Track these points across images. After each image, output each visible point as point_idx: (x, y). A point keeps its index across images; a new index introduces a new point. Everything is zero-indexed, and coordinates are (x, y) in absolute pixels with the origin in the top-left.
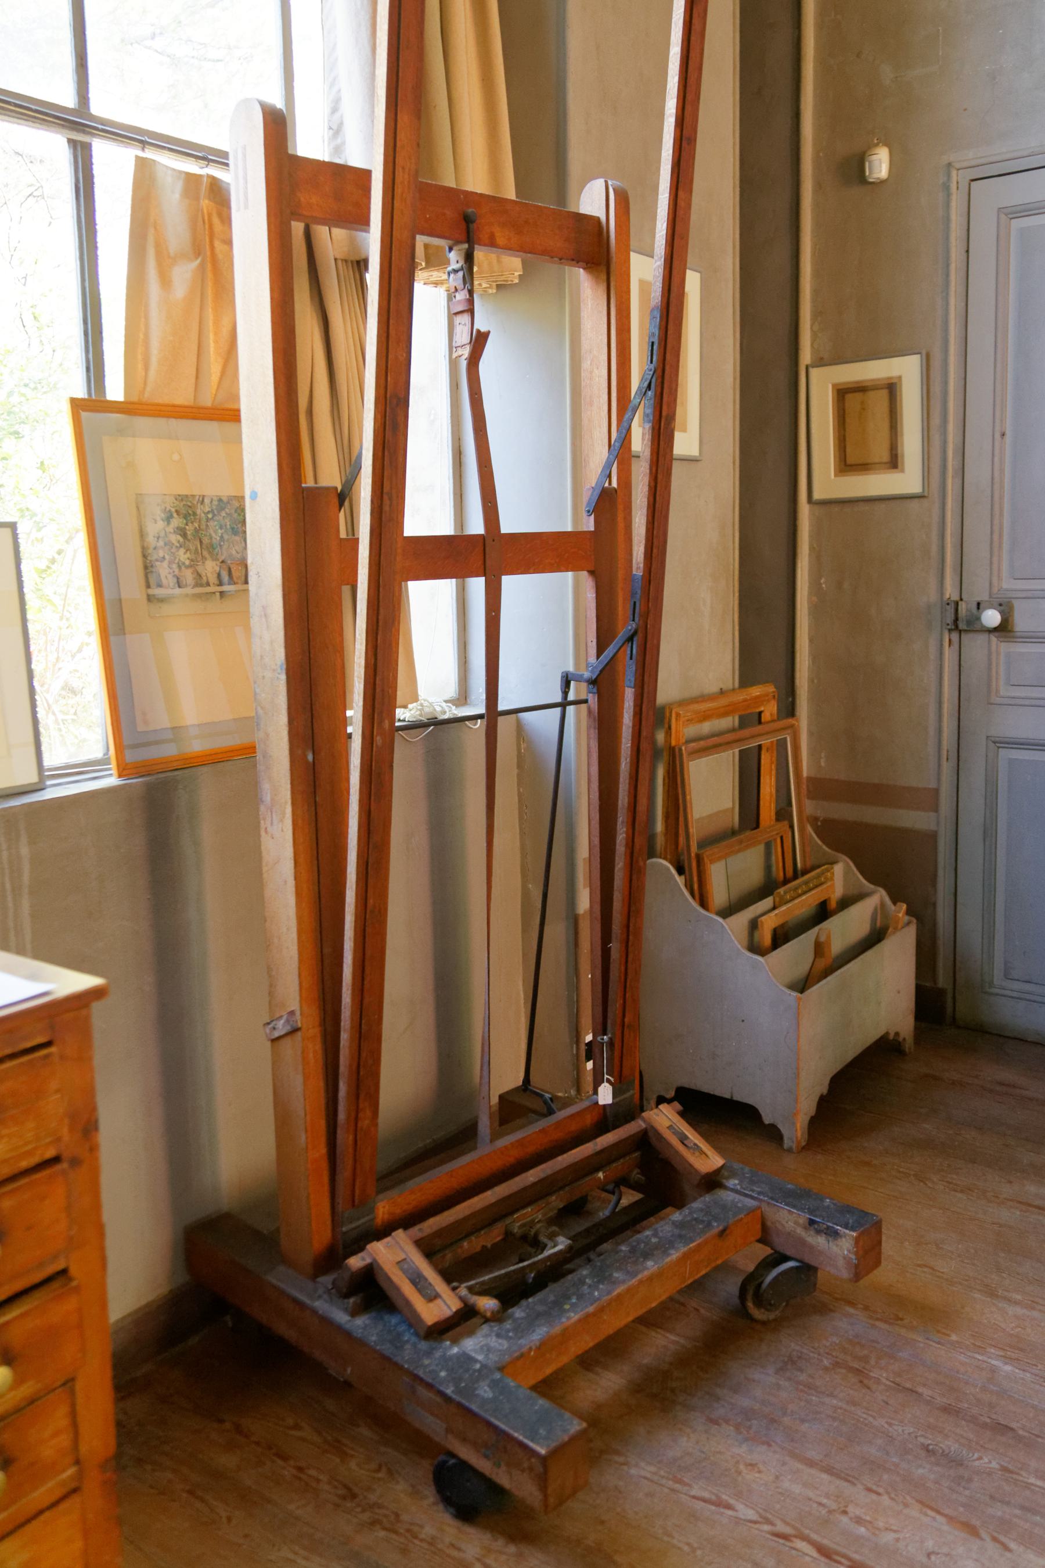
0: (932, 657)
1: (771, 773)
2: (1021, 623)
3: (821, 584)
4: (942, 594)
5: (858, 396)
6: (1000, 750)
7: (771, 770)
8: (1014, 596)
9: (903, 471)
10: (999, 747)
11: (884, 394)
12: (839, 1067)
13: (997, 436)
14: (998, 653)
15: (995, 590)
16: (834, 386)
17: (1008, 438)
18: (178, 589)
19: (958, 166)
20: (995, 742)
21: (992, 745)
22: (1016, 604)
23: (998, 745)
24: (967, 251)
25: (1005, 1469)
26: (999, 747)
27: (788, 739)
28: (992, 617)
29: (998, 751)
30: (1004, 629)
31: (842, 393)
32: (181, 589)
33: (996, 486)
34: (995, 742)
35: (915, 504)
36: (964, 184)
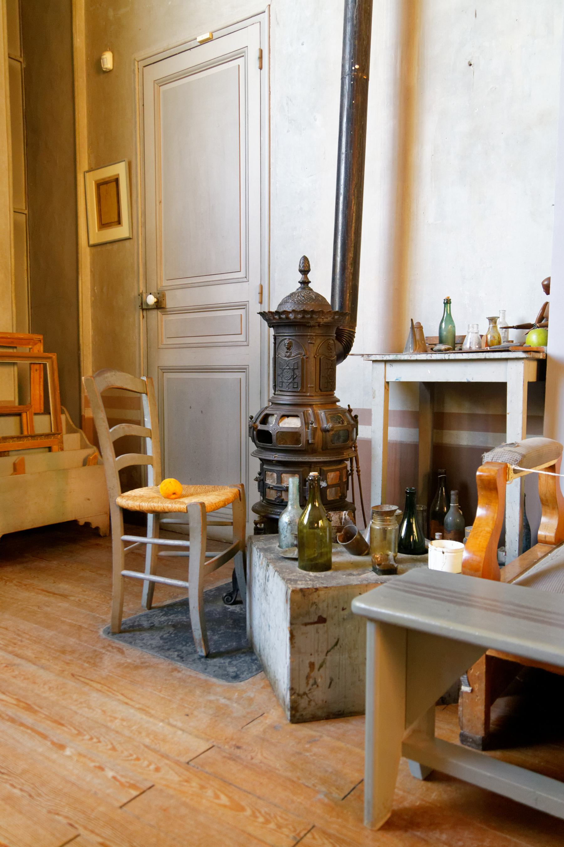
0: (137, 325)
1: (40, 384)
2: (169, 303)
3: (95, 290)
4: (139, 291)
5: (105, 186)
6: (164, 373)
7: (40, 382)
8: (166, 289)
9: (122, 226)
10: (163, 372)
11: (114, 183)
12: (12, 531)
13: (158, 203)
14: (162, 321)
15: (159, 287)
16: (95, 182)
17: (163, 204)
18: (206, 503)
19: (137, 59)
20: (162, 370)
21: (160, 371)
22: (167, 293)
23: (163, 371)
24: (143, 105)
25: (80, 755)
26: (163, 372)
27: (48, 365)
28: (151, 300)
29: (163, 375)
30: (159, 306)
31: (100, 185)
32: (201, 501)
33: (158, 231)
34: (162, 370)
35: (127, 243)
36: (141, 68)
